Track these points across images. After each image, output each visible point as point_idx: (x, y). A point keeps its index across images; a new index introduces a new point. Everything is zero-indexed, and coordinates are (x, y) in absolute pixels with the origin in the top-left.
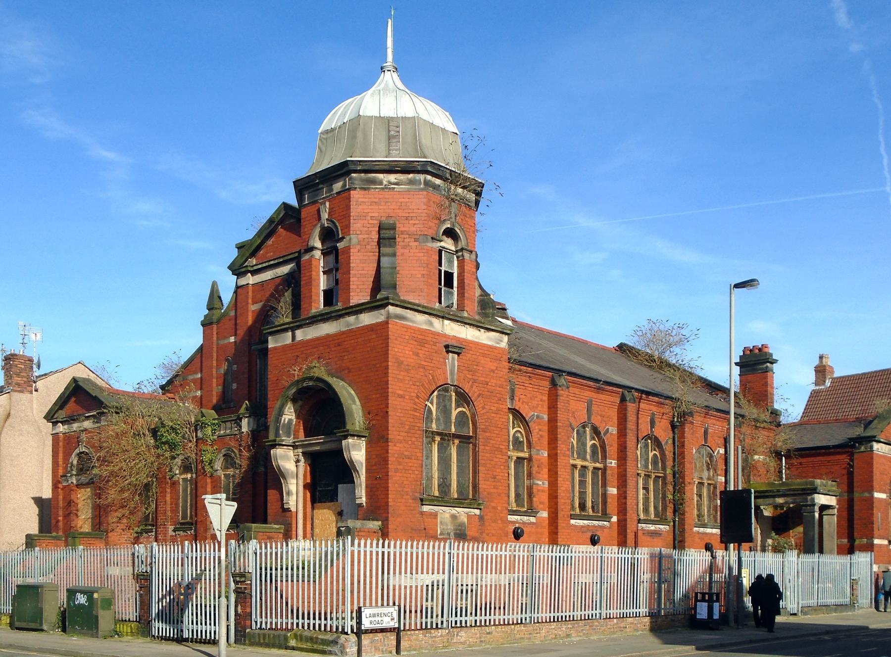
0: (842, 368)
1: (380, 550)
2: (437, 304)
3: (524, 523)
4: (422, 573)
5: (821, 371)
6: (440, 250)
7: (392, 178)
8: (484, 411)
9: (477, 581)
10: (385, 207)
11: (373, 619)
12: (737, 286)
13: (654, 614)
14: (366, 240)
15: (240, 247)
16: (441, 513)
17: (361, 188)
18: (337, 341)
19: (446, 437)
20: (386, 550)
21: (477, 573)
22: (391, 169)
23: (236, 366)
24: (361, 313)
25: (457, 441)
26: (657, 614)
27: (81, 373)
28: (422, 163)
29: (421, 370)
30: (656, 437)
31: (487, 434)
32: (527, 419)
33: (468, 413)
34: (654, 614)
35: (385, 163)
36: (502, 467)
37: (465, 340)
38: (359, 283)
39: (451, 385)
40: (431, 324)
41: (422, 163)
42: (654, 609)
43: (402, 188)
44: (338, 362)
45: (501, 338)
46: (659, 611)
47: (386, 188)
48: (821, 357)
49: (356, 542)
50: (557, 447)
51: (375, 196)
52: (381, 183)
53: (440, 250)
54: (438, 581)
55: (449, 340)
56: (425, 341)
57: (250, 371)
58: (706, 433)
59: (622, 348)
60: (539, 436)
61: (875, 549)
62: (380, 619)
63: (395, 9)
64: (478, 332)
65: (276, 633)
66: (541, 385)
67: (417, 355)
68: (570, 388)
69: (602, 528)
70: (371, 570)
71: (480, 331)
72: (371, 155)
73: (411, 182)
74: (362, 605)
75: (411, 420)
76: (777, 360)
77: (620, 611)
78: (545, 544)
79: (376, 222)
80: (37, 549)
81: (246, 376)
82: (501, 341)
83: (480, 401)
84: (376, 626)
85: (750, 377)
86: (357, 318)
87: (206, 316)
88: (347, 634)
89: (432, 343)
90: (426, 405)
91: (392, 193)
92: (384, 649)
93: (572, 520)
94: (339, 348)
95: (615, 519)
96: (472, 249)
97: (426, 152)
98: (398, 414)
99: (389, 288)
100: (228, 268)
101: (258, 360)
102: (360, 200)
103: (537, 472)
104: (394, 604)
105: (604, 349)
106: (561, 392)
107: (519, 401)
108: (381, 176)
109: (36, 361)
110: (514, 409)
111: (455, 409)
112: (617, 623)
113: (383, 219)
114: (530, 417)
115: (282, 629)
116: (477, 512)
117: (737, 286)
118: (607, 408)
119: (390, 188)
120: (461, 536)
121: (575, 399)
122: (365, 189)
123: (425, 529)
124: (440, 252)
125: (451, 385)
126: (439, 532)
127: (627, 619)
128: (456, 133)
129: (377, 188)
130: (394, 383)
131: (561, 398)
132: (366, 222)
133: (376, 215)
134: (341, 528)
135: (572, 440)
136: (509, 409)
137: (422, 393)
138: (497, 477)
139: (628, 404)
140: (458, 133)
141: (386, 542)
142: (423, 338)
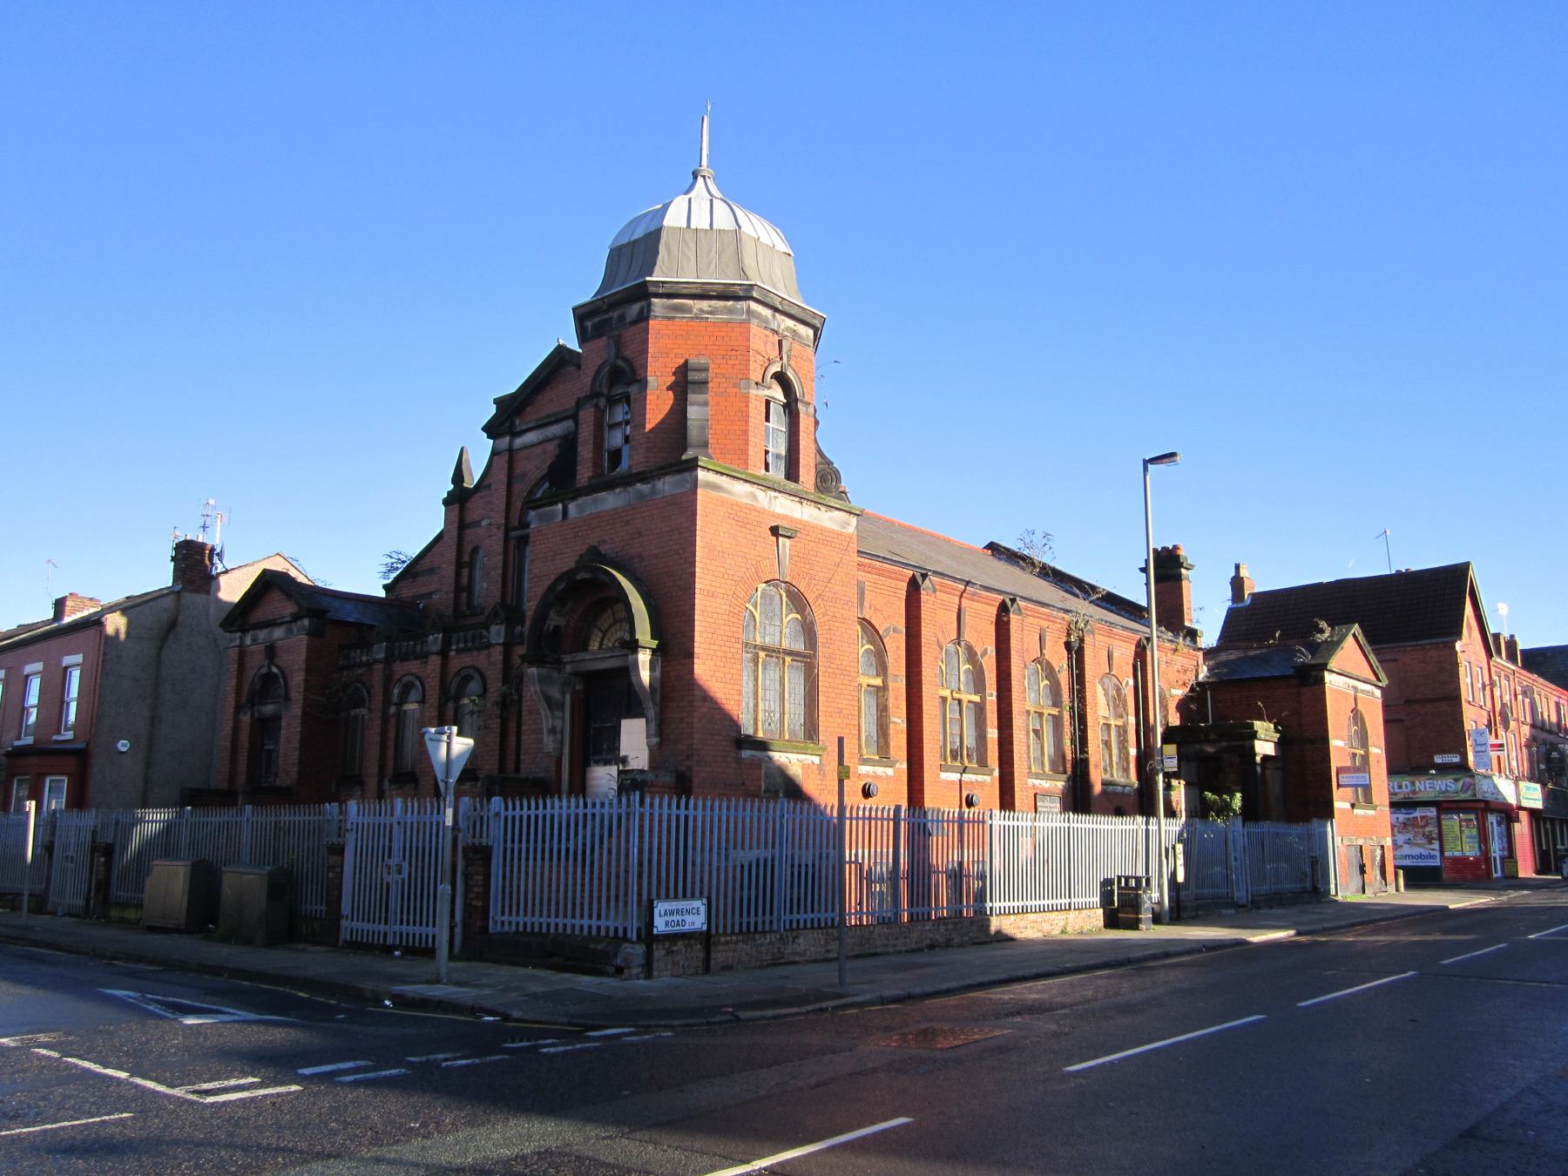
0: (1260, 582)
1: (683, 812)
2: (763, 471)
3: (876, 777)
5: (1237, 583)
6: (766, 400)
9: (814, 860)
11: (669, 918)
13: (887, 920)
15: (496, 401)
16: (767, 762)
26: (892, 919)
27: (278, 565)
28: (744, 287)
30: (1048, 663)
32: (881, 632)
34: (887, 920)
35: (696, 286)
36: (850, 698)
37: (800, 522)
39: (781, 582)
41: (744, 287)
42: (887, 912)
43: (717, 318)
45: (849, 520)
46: (897, 915)
47: (697, 318)
48: (1237, 567)
49: (648, 800)
53: (766, 400)
54: (758, 861)
56: (745, 521)
58: (1110, 657)
60: (896, 656)
62: (680, 918)
63: (713, 104)
64: (817, 510)
66: (898, 587)
69: (982, 784)
70: (668, 844)
71: (819, 509)
74: (654, 895)
76: (1193, 566)
77: (1023, 904)
81: (500, 571)
82: (848, 524)
83: (819, 605)
84: (675, 928)
88: (630, 941)
89: (755, 523)
90: (747, 608)
91: (704, 324)
92: (686, 965)
93: (942, 773)
96: (809, 401)
97: (749, 274)
99: (698, 446)
100: (482, 429)
103: (894, 706)
104: (701, 893)
107: (870, 608)
108: (690, 302)
109: (218, 550)
110: (864, 619)
111: (786, 616)
114: (885, 631)
116: (816, 760)
118: (984, 621)
119: (702, 318)
121: (944, 607)
122: (669, 318)
123: (743, 784)
124: (768, 403)
125: (781, 582)
126: (763, 788)
127: (1028, 915)
128: (789, 255)
130: (704, 576)
134: (625, 782)
135: (940, 663)
136: (859, 618)
137: (742, 592)
140: (791, 253)
141: (692, 801)
142: (742, 516)
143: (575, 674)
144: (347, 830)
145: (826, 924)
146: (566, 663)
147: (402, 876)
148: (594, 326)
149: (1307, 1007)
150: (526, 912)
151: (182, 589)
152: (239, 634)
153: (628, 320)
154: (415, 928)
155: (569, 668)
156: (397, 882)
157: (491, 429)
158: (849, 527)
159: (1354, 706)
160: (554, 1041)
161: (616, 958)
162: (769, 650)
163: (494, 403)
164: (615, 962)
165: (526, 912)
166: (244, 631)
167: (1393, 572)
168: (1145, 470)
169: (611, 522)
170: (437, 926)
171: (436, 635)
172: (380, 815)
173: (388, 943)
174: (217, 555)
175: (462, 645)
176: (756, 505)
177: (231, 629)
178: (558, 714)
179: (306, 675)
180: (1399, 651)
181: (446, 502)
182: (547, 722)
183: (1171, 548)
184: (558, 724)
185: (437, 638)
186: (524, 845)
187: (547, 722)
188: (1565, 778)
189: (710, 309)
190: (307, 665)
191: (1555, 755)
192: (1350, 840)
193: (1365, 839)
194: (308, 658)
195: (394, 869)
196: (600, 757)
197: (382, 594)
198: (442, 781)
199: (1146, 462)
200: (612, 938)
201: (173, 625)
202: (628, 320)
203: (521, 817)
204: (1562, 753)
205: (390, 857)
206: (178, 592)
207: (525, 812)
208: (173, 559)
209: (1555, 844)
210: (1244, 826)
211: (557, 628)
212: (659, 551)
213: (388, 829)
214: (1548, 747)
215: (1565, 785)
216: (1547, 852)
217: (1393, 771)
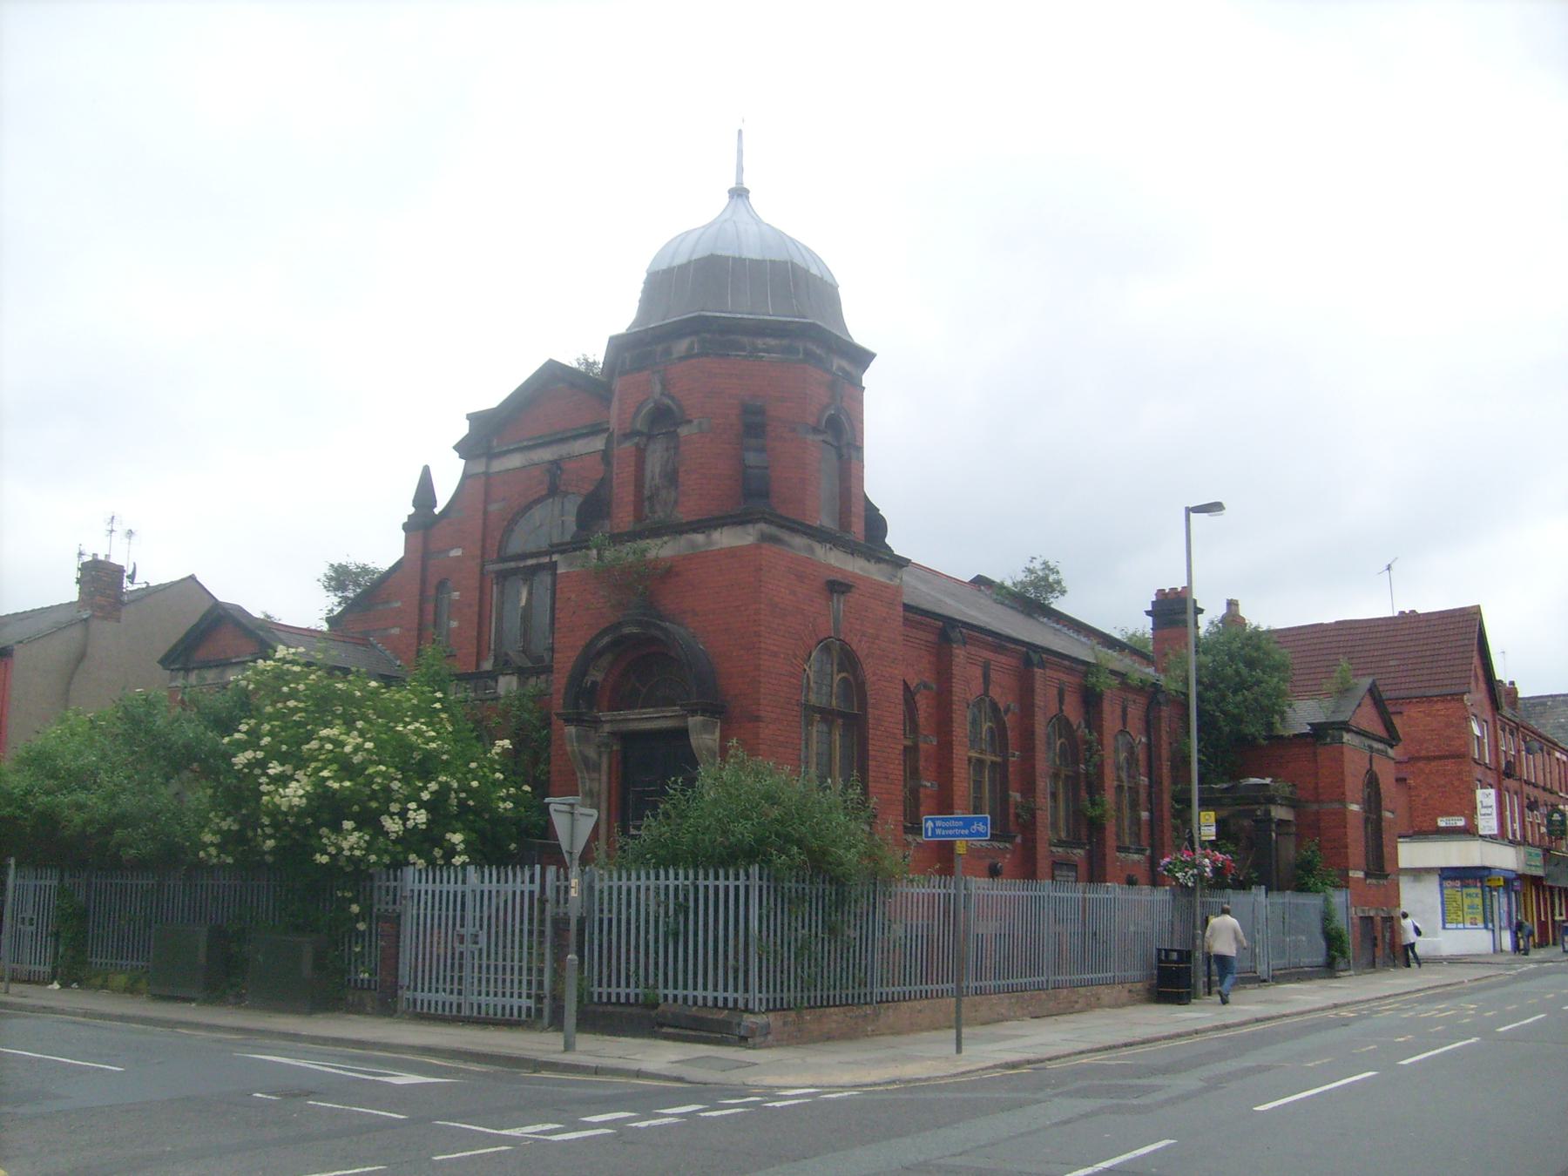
23: (458, 593)
25: (840, 721)
33: (851, 679)
37: (855, 576)
40: (812, 550)
50: (952, 731)
57: (481, 600)
59: (980, 581)
61: (1351, 883)
65: (600, 1009)
68: (967, 646)
72: (730, 309)
95: (1018, 840)
101: (495, 587)
106: (958, 651)
115: (628, 1003)
129: (738, 355)
131: (957, 660)
138: (891, 777)
139: (1036, 670)
143: (612, 734)
144: (405, 898)
145: (893, 998)
146: (604, 722)
147: (479, 946)
151: (93, 616)
153: (675, 355)
154: (488, 998)
155: (607, 728)
156: (473, 953)
157: (463, 448)
158: (896, 579)
159: (1369, 767)
160: (557, 1126)
162: (821, 710)
163: (468, 418)
166: (187, 670)
167: (1396, 614)
170: (1461, 980)
172: (449, 882)
174: (128, 577)
178: (595, 775)
180: (1410, 702)
181: (406, 527)
183: (1179, 589)
184: (595, 786)
186: (436, 913)
188: (1564, 842)
189: (764, 346)
191: (1556, 817)
192: (1363, 911)
193: (1377, 909)
195: (468, 939)
197: (325, 627)
198: (567, 851)
199: (1189, 510)
201: (82, 656)
202: (675, 355)
203: (620, 888)
204: (1563, 814)
205: (462, 926)
206: (86, 620)
207: (672, 883)
208: (79, 581)
209: (1553, 915)
210: (1266, 897)
211: (594, 683)
213: (459, 899)
214: (1549, 807)
215: (1564, 850)
216: (1546, 923)
217: (1199, 784)
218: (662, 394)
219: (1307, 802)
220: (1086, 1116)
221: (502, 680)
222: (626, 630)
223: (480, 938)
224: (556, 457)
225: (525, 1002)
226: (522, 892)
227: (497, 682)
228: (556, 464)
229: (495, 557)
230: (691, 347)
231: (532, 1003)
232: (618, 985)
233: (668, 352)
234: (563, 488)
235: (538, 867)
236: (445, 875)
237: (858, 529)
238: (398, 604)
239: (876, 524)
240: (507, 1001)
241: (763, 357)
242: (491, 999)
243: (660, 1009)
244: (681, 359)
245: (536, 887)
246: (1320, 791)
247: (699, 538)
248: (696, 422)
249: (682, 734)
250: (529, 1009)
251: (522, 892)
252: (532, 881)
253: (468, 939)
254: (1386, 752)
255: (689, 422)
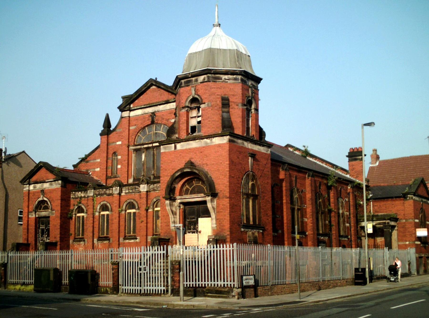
4: (243, 261)
7: (226, 77)
8: (263, 183)
10: (223, 90)
12: (365, 125)
14: (215, 105)
15: (123, 98)
17: (212, 81)
18: (200, 151)
19: (248, 196)
20: (225, 249)
21: (262, 260)
22: (226, 73)
24: (214, 137)
25: (251, 198)
29: (240, 165)
31: (264, 194)
37: (255, 151)
38: (212, 124)
40: (243, 144)
44: (201, 161)
51: (219, 85)
52: (221, 79)
55: (250, 151)
67: (238, 158)
72: (216, 66)
73: (235, 79)
75: (237, 188)
78: (291, 245)
79: (219, 97)
80: (320, 247)
85: (354, 163)
86: (211, 140)
87: (102, 131)
94: (201, 154)
98: (232, 186)
102: (212, 87)
105: (281, 147)
109: (4, 150)
112: (327, 283)
113: (223, 95)
117: (365, 125)
120: (255, 242)
122: (214, 81)
132: (215, 96)
133: (219, 93)
138: (268, 214)
143: (181, 203)
147: (147, 271)
148: (185, 82)
149: (422, 299)
150: (221, 279)
152: (28, 185)
155: (179, 201)
161: (232, 292)
164: (232, 294)
165: (221, 279)
166: (30, 184)
168: (363, 128)
169: (223, 163)
171: (116, 188)
173: (142, 293)
175: (127, 191)
176: (244, 146)
177: (25, 183)
179: (61, 202)
182: (172, 219)
183: (358, 148)
185: (117, 188)
187: (172, 219)
190: (61, 197)
194: (61, 195)
196: (191, 231)
197: (72, 168)
200: (223, 287)
205: (141, 265)
212: (214, 162)
218: (195, 94)
219: (401, 219)
220: (343, 311)
221: (142, 186)
222: (185, 170)
223: (146, 269)
224: (153, 111)
225: (163, 288)
226: (161, 254)
227: (139, 187)
228: (153, 114)
229: (133, 144)
230: (204, 79)
231: (165, 288)
232: (202, 281)
233: (196, 80)
234: (156, 122)
235: (165, 246)
236: (134, 249)
237: (253, 132)
238: (99, 160)
239: (261, 133)
240: (157, 288)
241: (227, 82)
242: (149, 288)
243: (207, 288)
244: (201, 83)
245: (165, 252)
246: (406, 215)
247: (208, 141)
248: (206, 103)
249: (205, 202)
250: (164, 290)
251: (161, 254)
252: (164, 250)
253: (142, 269)
254: (427, 202)
255: (204, 103)
